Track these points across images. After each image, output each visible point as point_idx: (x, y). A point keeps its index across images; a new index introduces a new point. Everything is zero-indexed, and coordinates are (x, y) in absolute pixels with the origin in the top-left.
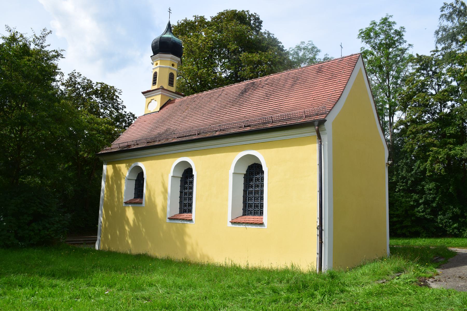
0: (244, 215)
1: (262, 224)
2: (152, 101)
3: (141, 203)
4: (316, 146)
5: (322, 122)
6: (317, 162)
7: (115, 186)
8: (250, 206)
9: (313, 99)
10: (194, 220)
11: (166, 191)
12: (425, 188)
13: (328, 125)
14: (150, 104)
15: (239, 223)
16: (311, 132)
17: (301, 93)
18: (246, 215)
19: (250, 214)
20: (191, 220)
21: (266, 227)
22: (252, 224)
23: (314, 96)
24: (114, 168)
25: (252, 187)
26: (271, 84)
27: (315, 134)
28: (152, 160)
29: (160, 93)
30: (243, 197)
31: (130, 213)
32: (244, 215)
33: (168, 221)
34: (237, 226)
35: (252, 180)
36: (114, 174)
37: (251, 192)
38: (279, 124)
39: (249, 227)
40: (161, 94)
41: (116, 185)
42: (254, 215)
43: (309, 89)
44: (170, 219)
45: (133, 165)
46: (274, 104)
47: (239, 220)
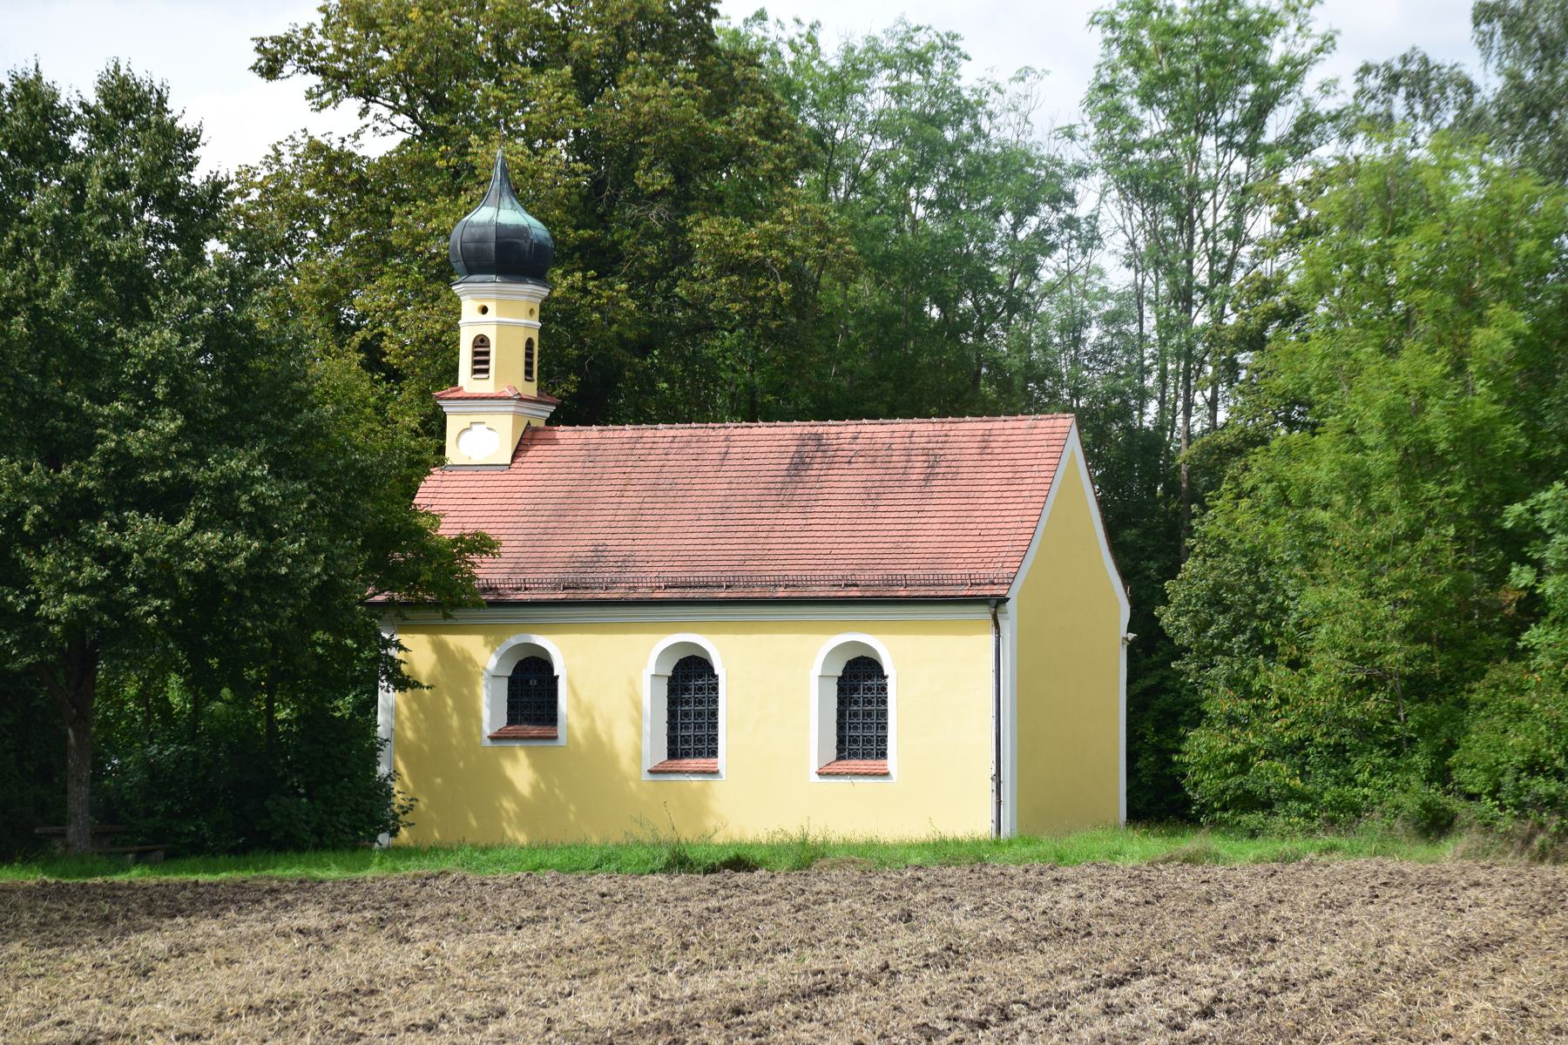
0: (839, 759)
1: (886, 775)
2: (474, 427)
3: (555, 738)
4: (991, 638)
5: (1002, 601)
6: (993, 666)
7: (450, 702)
8: (855, 740)
9: (977, 532)
10: (723, 772)
11: (637, 705)
12: (1476, 503)
13: (1011, 606)
14: (466, 435)
15: (828, 774)
16: (984, 613)
17: (950, 507)
18: (844, 758)
19: (854, 755)
20: (715, 773)
21: (895, 780)
22: (866, 775)
23: (980, 526)
24: (441, 650)
25: (856, 703)
26: (873, 456)
27: (990, 617)
28: (582, 632)
29: (512, 409)
30: (838, 723)
31: (520, 769)
32: (839, 759)
33: (646, 777)
34: (833, 781)
35: (856, 689)
36: (443, 666)
37: (856, 714)
38: (922, 592)
39: (861, 781)
40: (515, 413)
41: (451, 697)
42: (863, 758)
43: (966, 501)
44: (651, 772)
45: (513, 640)
46: (892, 527)
47: (836, 768)
